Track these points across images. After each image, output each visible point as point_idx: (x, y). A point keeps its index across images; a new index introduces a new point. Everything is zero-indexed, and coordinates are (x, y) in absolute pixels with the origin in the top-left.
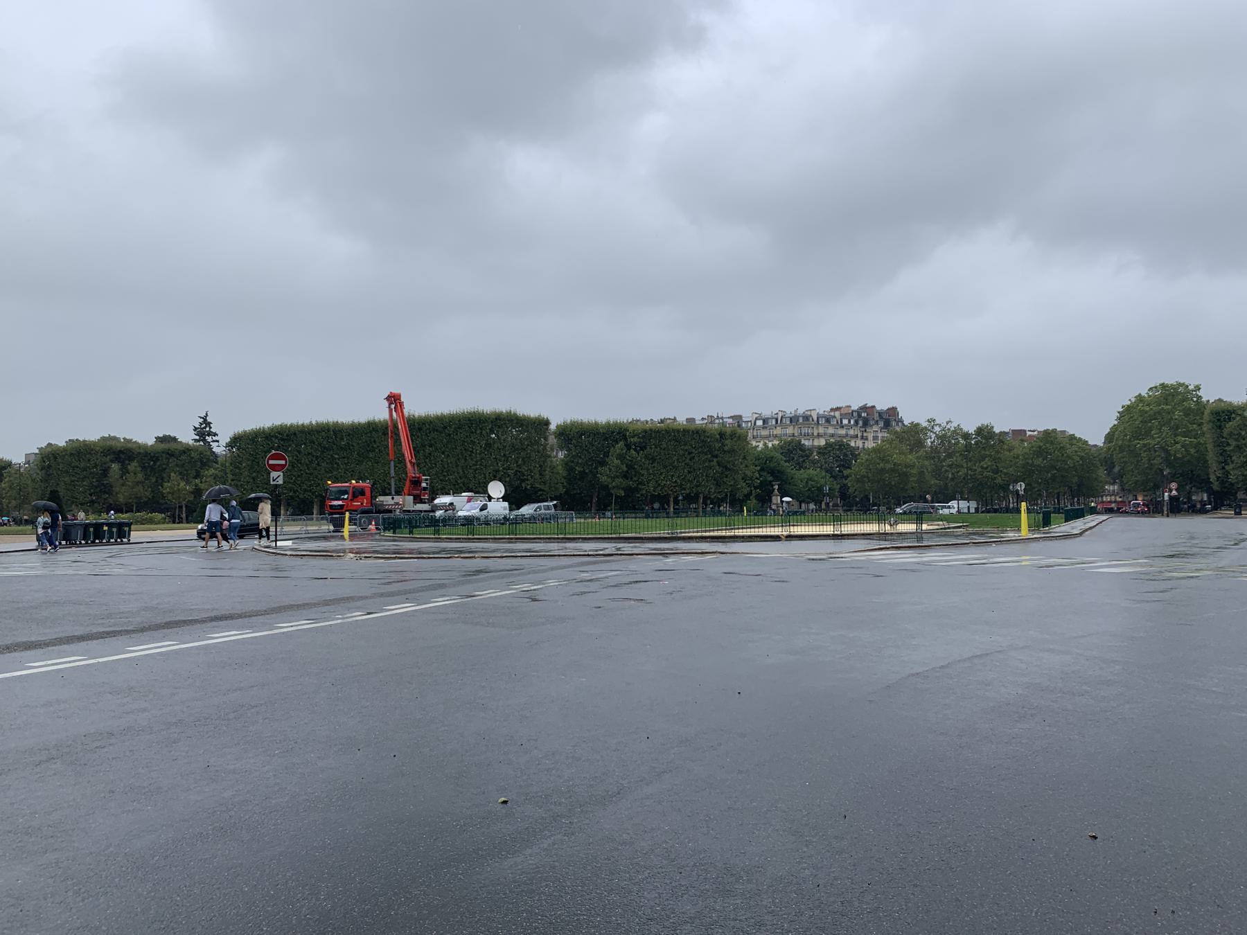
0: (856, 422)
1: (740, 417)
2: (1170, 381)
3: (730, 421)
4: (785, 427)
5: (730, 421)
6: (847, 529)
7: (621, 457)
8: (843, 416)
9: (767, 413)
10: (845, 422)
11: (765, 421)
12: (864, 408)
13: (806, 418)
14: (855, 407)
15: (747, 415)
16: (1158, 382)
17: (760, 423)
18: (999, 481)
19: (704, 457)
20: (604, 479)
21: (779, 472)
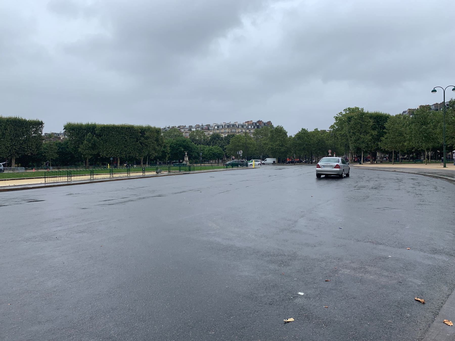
0: (254, 127)
1: (209, 125)
2: (353, 107)
3: (206, 127)
4: (225, 129)
5: (206, 127)
6: (75, 179)
7: (89, 141)
8: (249, 125)
9: (219, 123)
10: (250, 127)
11: (218, 127)
12: (259, 122)
13: (233, 125)
14: (256, 121)
15: (211, 124)
16: (347, 107)
17: (216, 127)
18: (282, 150)
19: (132, 140)
20: (80, 150)
21: (188, 147)
